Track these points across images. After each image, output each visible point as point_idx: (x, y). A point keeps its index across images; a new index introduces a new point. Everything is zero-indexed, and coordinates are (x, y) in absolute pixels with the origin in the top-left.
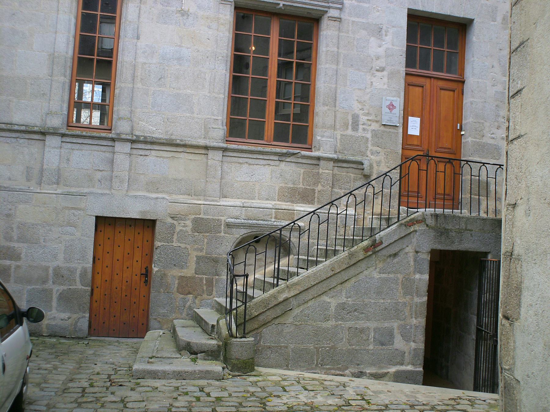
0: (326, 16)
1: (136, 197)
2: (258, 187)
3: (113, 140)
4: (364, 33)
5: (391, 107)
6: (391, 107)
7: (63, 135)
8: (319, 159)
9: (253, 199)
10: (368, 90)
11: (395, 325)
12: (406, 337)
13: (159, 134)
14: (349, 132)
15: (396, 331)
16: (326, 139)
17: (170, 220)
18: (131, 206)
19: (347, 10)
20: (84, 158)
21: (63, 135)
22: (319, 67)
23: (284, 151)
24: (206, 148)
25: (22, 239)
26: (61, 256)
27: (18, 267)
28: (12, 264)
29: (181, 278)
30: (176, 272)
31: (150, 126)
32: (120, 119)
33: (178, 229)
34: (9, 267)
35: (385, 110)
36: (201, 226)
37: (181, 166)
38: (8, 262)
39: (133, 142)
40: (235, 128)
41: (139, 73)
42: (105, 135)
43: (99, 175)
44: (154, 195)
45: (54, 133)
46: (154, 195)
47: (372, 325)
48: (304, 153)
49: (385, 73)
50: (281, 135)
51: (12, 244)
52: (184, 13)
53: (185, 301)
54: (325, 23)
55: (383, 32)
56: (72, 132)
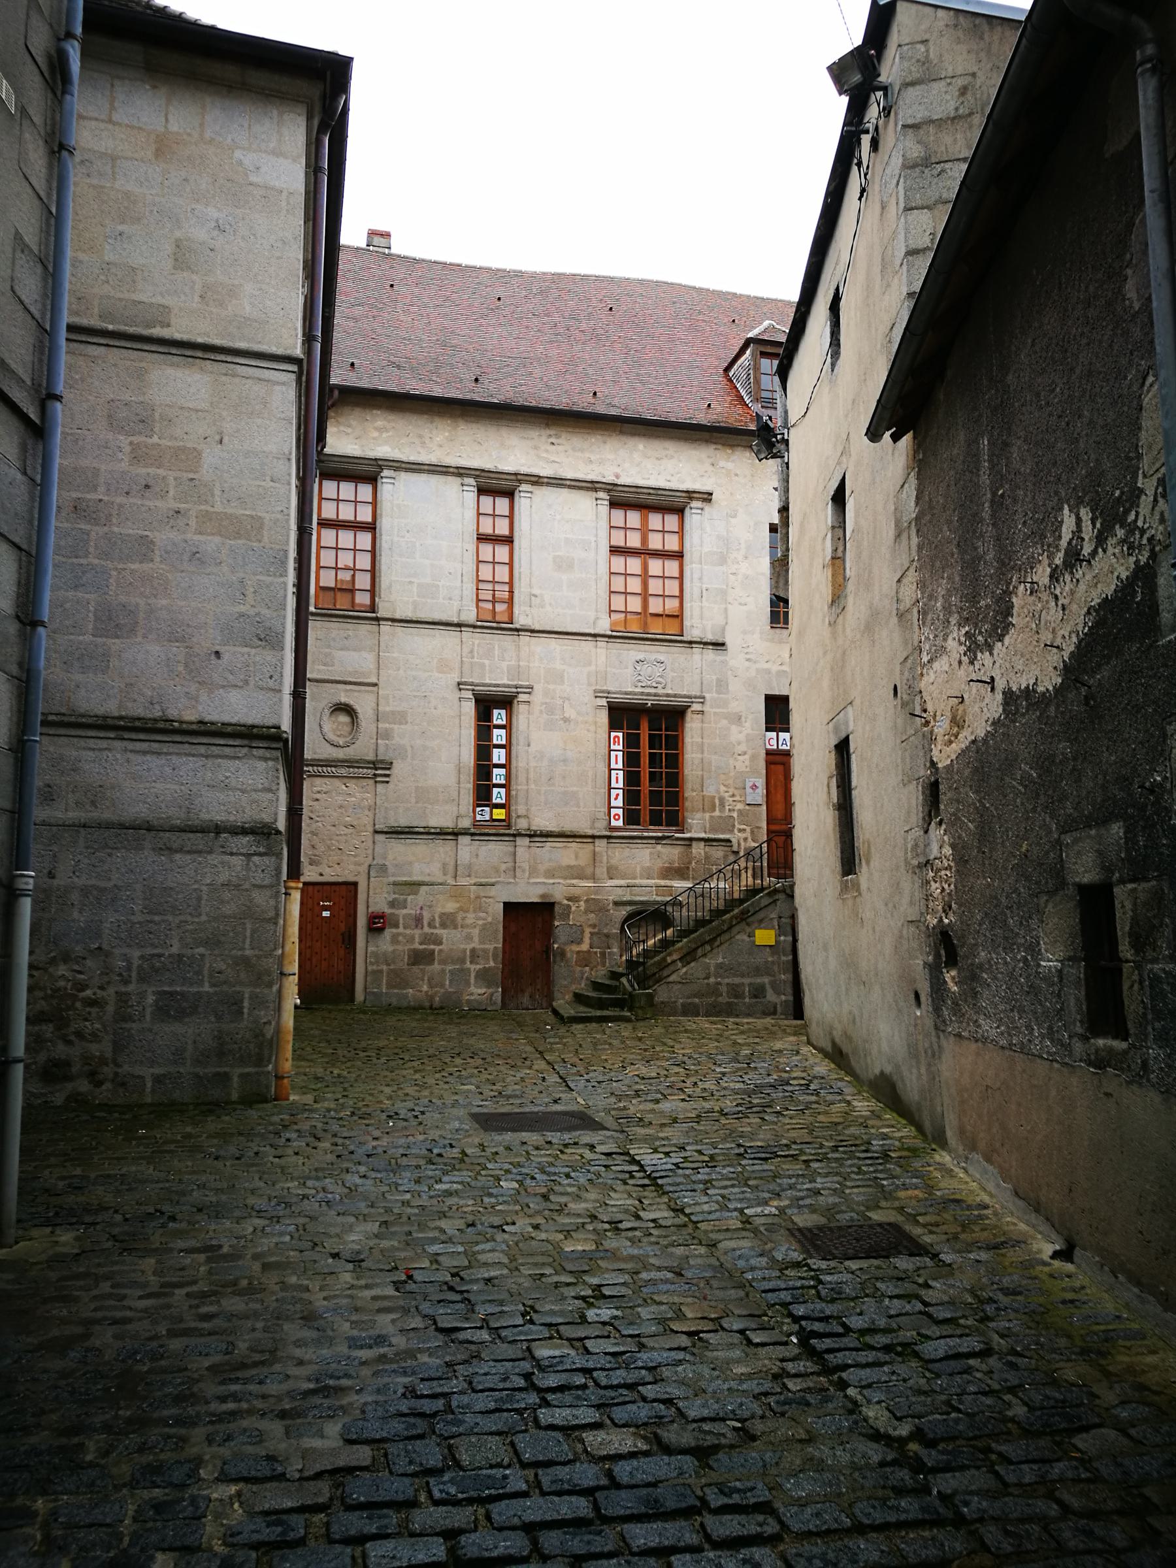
0: (689, 710)
1: (537, 883)
2: (641, 870)
3: (514, 835)
4: (725, 722)
5: (754, 787)
6: (754, 787)
7: (472, 834)
8: (691, 839)
9: (635, 878)
10: (732, 774)
11: (766, 980)
12: (778, 993)
13: (552, 827)
14: (717, 813)
15: (768, 987)
16: (697, 824)
17: (566, 902)
18: (528, 892)
19: (708, 703)
20: (493, 852)
21: (472, 834)
22: (686, 756)
23: (660, 834)
24: (593, 837)
25: (443, 925)
26: (476, 939)
27: (441, 951)
28: (437, 948)
29: (578, 952)
30: (575, 948)
31: (543, 821)
32: (518, 817)
33: (573, 908)
34: (433, 951)
35: (749, 790)
36: (596, 906)
37: (568, 855)
38: (432, 947)
39: (530, 836)
40: (631, 818)
41: (532, 775)
42: (505, 831)
43: (503, 867)
44: (551, 881)
45: (465, 832)
46: (551, 881)
47: (747, 981)
48: (677, 835)
49: (747, 757)
50: (656, 820)
51: (435, 931)
52: (566, 720)
53: (583, 973)
54: (689, 716)
55: (743, 719)
56: (478, 832)
